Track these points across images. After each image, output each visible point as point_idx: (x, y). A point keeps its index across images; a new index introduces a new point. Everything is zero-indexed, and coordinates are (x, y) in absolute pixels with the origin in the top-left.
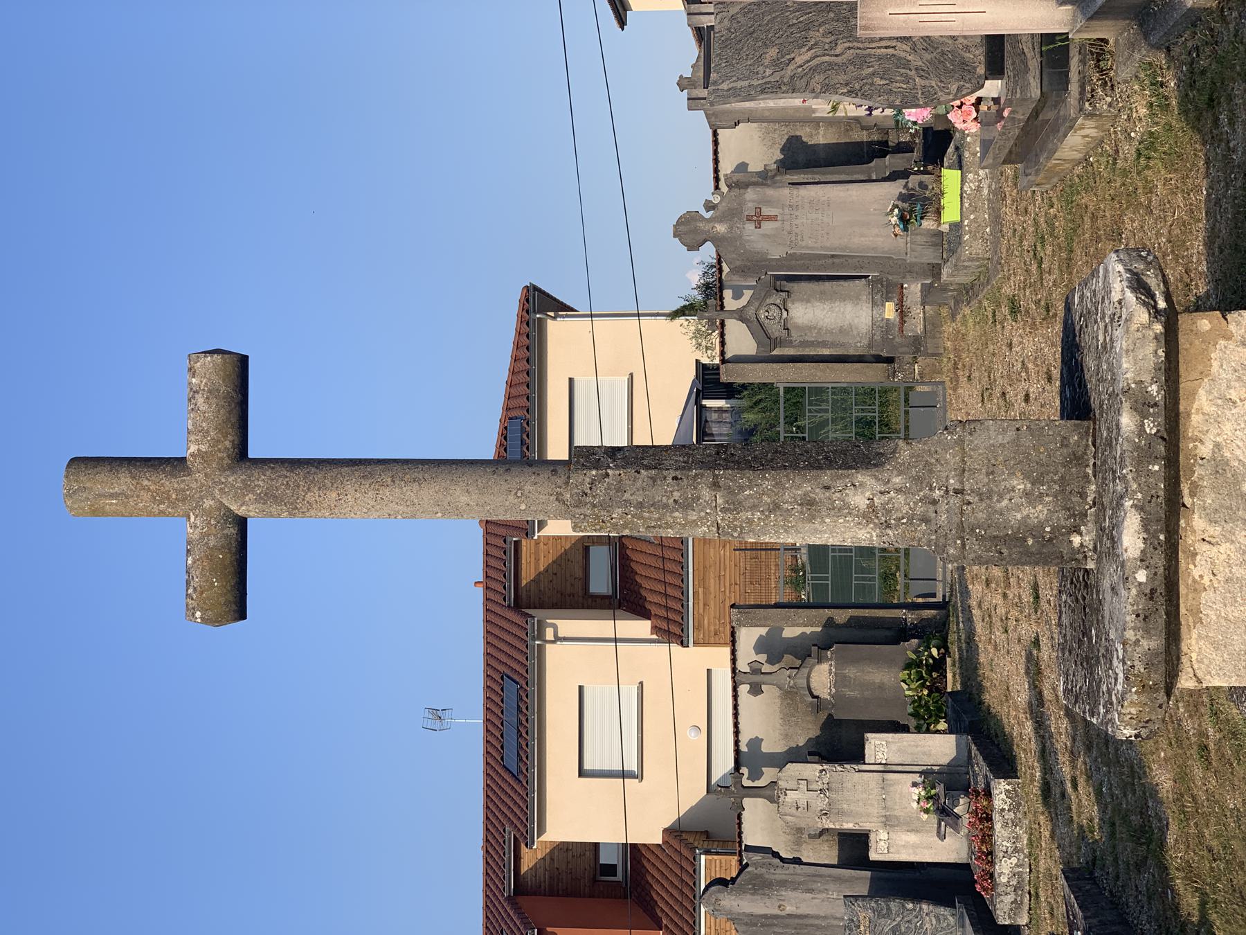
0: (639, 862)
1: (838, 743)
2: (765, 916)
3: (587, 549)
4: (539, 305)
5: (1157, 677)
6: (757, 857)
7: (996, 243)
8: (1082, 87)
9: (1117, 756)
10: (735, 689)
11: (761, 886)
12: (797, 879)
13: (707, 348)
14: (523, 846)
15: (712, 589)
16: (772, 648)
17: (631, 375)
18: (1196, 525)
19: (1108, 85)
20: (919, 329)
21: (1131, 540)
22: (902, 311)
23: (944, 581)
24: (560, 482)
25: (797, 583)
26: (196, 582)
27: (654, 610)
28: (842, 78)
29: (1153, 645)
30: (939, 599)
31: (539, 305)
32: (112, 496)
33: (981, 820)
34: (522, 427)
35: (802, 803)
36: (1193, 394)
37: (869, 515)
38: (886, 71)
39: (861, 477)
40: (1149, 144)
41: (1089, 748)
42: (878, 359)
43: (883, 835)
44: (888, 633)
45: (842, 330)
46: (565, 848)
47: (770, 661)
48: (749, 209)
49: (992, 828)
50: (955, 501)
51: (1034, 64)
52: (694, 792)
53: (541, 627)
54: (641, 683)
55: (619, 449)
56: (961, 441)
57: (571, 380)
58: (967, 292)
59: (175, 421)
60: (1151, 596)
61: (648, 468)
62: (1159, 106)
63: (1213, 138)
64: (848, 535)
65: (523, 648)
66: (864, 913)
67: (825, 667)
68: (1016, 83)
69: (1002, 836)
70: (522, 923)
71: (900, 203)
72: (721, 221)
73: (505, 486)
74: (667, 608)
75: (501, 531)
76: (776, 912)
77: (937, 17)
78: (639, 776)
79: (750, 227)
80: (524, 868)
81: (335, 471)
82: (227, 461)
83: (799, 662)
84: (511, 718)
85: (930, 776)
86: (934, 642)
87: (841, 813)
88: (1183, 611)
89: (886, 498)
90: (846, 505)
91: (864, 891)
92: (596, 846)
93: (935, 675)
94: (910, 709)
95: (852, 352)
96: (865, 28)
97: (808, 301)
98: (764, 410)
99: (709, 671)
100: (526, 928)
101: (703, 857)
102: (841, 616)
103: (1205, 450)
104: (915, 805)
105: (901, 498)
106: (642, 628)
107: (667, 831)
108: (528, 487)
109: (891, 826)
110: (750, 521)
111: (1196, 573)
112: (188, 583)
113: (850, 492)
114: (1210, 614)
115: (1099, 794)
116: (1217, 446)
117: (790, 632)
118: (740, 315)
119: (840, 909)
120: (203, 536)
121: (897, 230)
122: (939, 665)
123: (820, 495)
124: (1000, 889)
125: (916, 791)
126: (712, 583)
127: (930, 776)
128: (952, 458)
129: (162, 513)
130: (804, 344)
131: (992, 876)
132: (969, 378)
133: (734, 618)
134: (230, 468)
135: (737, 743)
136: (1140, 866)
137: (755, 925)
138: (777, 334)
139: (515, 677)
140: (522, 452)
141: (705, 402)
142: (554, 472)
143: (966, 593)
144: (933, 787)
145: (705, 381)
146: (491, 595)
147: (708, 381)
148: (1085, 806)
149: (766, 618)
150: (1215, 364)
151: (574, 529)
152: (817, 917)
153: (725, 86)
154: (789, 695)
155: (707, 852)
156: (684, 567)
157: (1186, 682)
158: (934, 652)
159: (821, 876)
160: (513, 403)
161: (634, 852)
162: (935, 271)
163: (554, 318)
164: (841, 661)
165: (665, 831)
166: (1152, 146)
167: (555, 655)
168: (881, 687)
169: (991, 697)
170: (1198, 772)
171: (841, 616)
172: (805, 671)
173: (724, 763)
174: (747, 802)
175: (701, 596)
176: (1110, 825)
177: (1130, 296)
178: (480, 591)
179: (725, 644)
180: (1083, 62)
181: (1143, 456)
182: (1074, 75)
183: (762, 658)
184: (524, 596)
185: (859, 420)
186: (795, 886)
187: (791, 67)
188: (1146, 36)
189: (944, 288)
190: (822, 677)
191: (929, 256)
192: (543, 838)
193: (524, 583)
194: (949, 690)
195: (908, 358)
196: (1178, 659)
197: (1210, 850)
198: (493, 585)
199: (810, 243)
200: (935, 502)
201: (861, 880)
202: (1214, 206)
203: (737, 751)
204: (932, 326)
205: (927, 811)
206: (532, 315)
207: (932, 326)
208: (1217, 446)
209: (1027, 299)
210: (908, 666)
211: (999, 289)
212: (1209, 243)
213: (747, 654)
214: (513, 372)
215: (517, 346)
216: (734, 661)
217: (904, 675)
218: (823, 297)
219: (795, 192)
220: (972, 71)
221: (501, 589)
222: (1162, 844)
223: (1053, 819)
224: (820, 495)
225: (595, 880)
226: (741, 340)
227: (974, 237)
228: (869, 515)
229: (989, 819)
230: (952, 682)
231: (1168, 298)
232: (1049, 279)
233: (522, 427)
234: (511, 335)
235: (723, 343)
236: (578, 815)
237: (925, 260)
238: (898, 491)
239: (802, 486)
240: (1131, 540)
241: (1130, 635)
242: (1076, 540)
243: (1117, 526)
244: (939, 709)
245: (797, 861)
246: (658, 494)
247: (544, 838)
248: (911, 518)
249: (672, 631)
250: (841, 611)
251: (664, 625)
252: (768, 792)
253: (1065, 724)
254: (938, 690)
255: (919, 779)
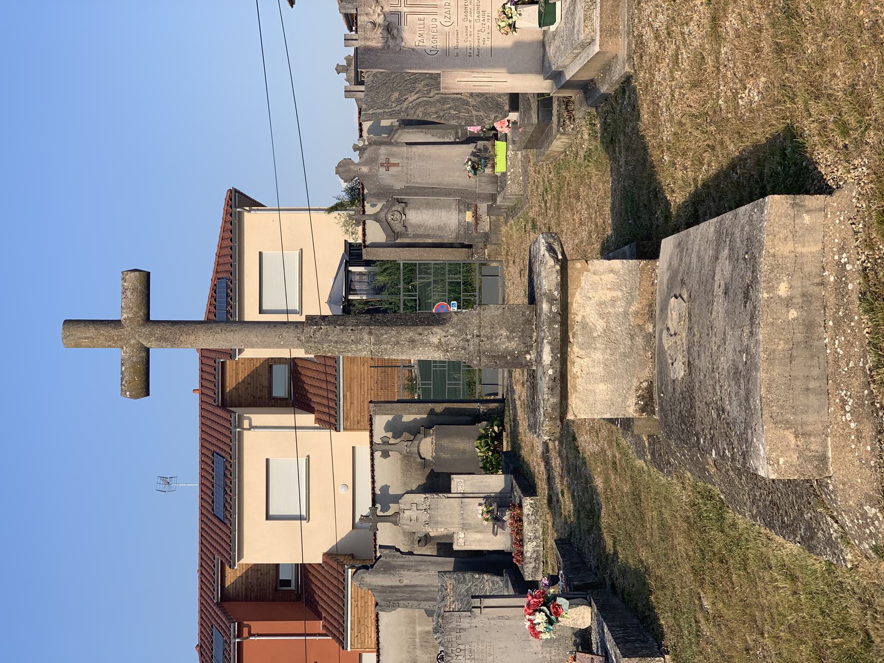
0: (307, 577)
1: (437, 483)
2: (391, 587)
3: (271, 367)
4: (239, 202)
5: (556, 414)
6: (387, 551)
7: (525, 186)
8: (559, 121)
9: (580, 474)
10: (372, 454)
11: (389, 569)
12: (410, 563)
13: (353, 233)
14: (227, 567)
15: (356, 393)
16: (396, 429)
17: (301, 250)
18: (575, 350)
19: (572, 118)
20: (487, 229)
21: (547, 358)
22: (476, 217)
23: (503, 385)
24: (299, 331)
25: (412, 388)
26: (127, 378)
27: (317, 407)
28: (433, 110)
29: (555, 400)
30: (500, 397)
31: (239, 202)
32: (86, 338)
33: (516, 521)
34: (227, 285)
35: (414, 518)
36: (574, 294)
37: (439, 346)
38: (457, 107)
39: (435, 329)
40: (588, 156)
41: (569, 472)
42: (463, 246)
43: (462, 535)
44: (468, 418)
45: (440, 228)
46: (256, 568)
47: (394, 437)
48: (382, 159)
49: (522, 526)
50: (477, 340)
51: (534, 106)
52: (345, 528)
53: (241, 419)
54: (308, 456)
55: (326, 316)
56: (479, 314)
57: (260, 253)
58: (512, 211)
59: (113, 304)
60: (554, 380)
61: (340, 325)
62: (593, 136)
63: (614, 159)
64: (430, 355)
65: (228, 433)
66: (450, 582)
67: (429, 439)
68: (525, 115)
69: (528, 530)
70: (227, 619)
71: (472, 158)
72: (364, 165)
73: (274, 334)
74: (328, 407)
75: (213, 355)
76: (398, 584)
77: (480, 84)
78: (307, 518)
79: (382, 170)
80: (228, 584)
81: (193, 327)
82: (141, 322)
83: (412, 437)
84: (219, 481)
85: (489, 499)
86: (496, 423)
87: (436, 523)
88: (569, 386)
89: (446, 339)
90: (429, 342)
91: (450, 568)
92: (277, 566)
93: (496, 443)
94: (481, 465)
95: (446, 241)
96: (445, 88)
97: (419, 209)
98: (390, 274)
99: (354, 448)
100: (230, 622)
101: (350, 570)
102: (439, 408)
103: (579, 318)
104: (480, 516)
105: (453, 339)
106: (308, 419)
107: (327, 555)
108: (285, 334)
109: (466, 529)
110: (386, 349)
111: (574, 370)
112: (122, 379)
113: (431, 336)
114: (580, 388)
115: (573, 496)
116: (583, 316)
117: (407, 418)
118: (376, 217)
119: (436, 581)
120: (130, 357)
121: (470, 174)
122: (498, 437)
123: (417, 337)
124: (527, 560)
125: (481, 508)
126: (356, 389)
127: (489, 499)
128: (475, 321)
129: (110, 346)
130: (416, 236)
131: (522, 553)
132: (514, 262)
133: (372, 409)
134: (143, 325)
135: (373, 488)
136: (590, 531)
137: (385, 592)
138: (399, 230)
139: (223, 454)
140: (227, 301)
141: (350, 268)
142: (297, 327)
143: (513, 391)
144: (491, 506)
145: (351, 254)
146: (205, 399)
147: (353, 254)
148: (567, 505)
149: (391, 409)
150: (583, 282)
151: (306, 352)
152: (422, 586)
153: (370, 112)
154: (407, 457)
155: (352, 567)
156: (336, 378)
157: (570, 417)
158: (496, 429)
159: (425, 562)
160: (220, 268)
161: (303, 569)
162: (493, 198)
163: (249, 211)
164: (439, 437)
165: (324, 554)
166: (590, 155)
167: (249, 437)
168: (464, 452)
169: (524, 452)
170: (613, 476)
171: (439, 408)
172: (416, 442)
173: (364, 507)
174: (380, 525)
175: (348, 398)
176: (577, 511)
177: (547, 254)
178: (197, 395)
179: (365, 429)
180: (559, 105)
181: (551, 321)
182: (555, 112)
183: (390, 434)
184: (228, 399)
185: (450, 283)
186: (408, 568)
187: (406, 103)
188: (586, 100)
189: (499, 208)
190: (427, 446)
191: (489, 189)
192: (241, 562)
193: (228, 390)
194: (505, 450)
195: (481, 245)
196: (567, 407)
197: (617, 515)
198: (206, 391)
199: (419, 180)
200: (468, 341)
201: (449, 563)
202: (614, 191)
203: (374, 494)
204: (495, 227)
205: (487, 520)
206: (233, 208)
207: (495, 227)
208: (583, 316)
209: (540, 221)
210: (480, 438)
211: (527, 213)
212: (612, 209)
213: (380, 432)
214: (221, 247)
215: (224, 230)
216: (371, 436)
217: (477, 443)
218: (429, 206)
219: (410, 149)
220: (502, 108)
221: (212, 394)
222: (599, 516)
223: (554, 516)
224: (417, 337)
225: (276, 590)
226: (376, 233)
227: (513, 182)
228: (439, 346)
229: (521, 520)
230: (506, 446)
231: (563, 254)
232: (550, 212)
233: (227, 285)
234: (219, 222)
235: (364, 235)
236: (266, 545)
237: (487, 192)
238: (452, 335)
239: (408, 333)
240: (547, 358)
241: (546, 396)
242: (528, 357)
243: (541, 351)
244: (498, 464)
245: (411, 553)
246: (344, 337)
247: (242, 561)
248: (458, 348)
249: (330, 421)
250: (439, 405)
251: (326, 418)
252: (393, 519)
253: (558, 461)
254: (498, 452)
255: (482, 501)
